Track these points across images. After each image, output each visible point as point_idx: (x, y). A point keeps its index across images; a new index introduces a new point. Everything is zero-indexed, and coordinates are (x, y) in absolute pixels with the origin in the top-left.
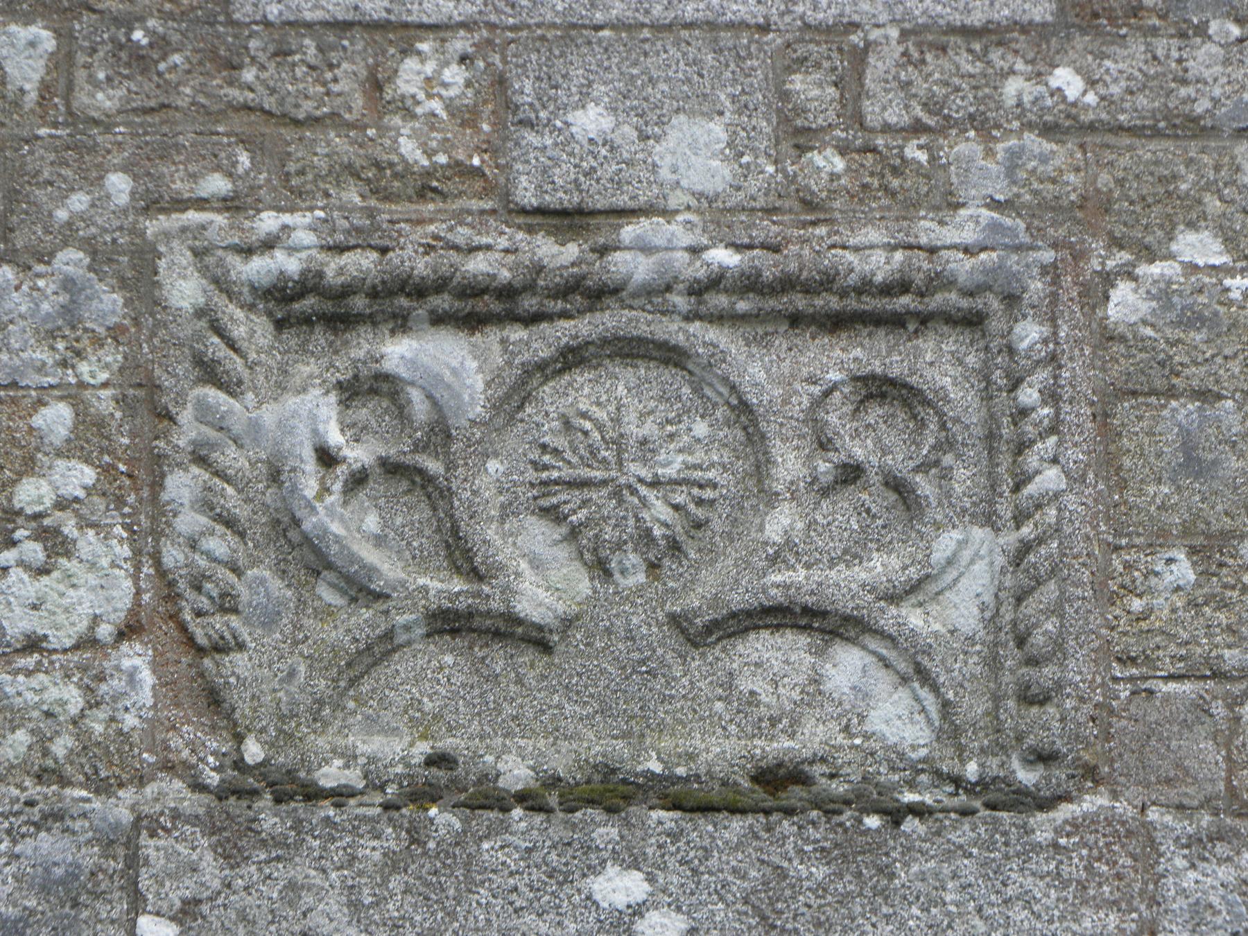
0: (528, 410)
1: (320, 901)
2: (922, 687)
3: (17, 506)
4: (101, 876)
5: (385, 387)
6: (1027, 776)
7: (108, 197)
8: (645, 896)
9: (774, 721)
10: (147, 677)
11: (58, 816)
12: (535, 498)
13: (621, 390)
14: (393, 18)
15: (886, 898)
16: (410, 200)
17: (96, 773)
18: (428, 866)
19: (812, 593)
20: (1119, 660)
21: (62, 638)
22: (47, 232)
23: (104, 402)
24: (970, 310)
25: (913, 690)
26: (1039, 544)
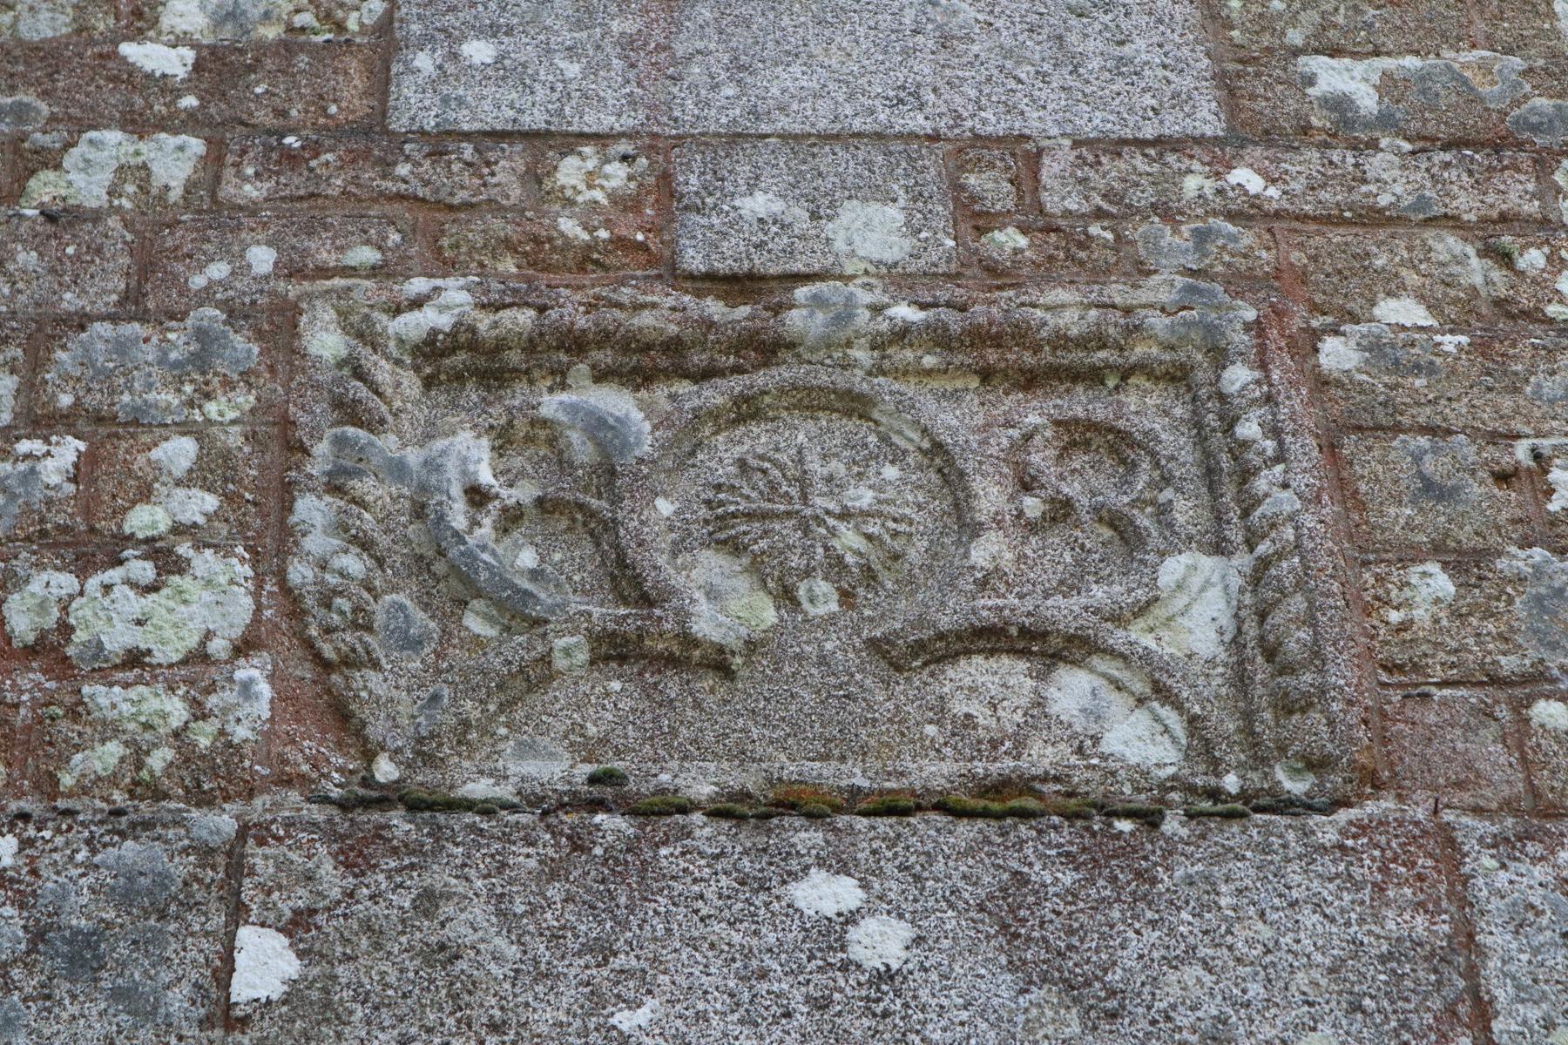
0: (700, 456)
1: (462, 911)
2: (1163, 706)
3: (127, 531)
4: (196, 886)
5: (543, 434)
6: (1296, 787)
7: (249, 266)
8: (859, 904)
9: (995, 744)
10: (265, 689)
11: (147, 825)
12: (710, 534)
13: (801, 437)
14: (553, 128)
15: (1149, 904)
16: (570, 271)
17: (199, 786)
18: (593, 873)
19: (1029, 614)
20: (1384, 668)
21: (168, 652)
22: (181, 294)
23: (234, 438)
24: (1173, 362)
25: (1152, 711)
26: (1279, 559)
